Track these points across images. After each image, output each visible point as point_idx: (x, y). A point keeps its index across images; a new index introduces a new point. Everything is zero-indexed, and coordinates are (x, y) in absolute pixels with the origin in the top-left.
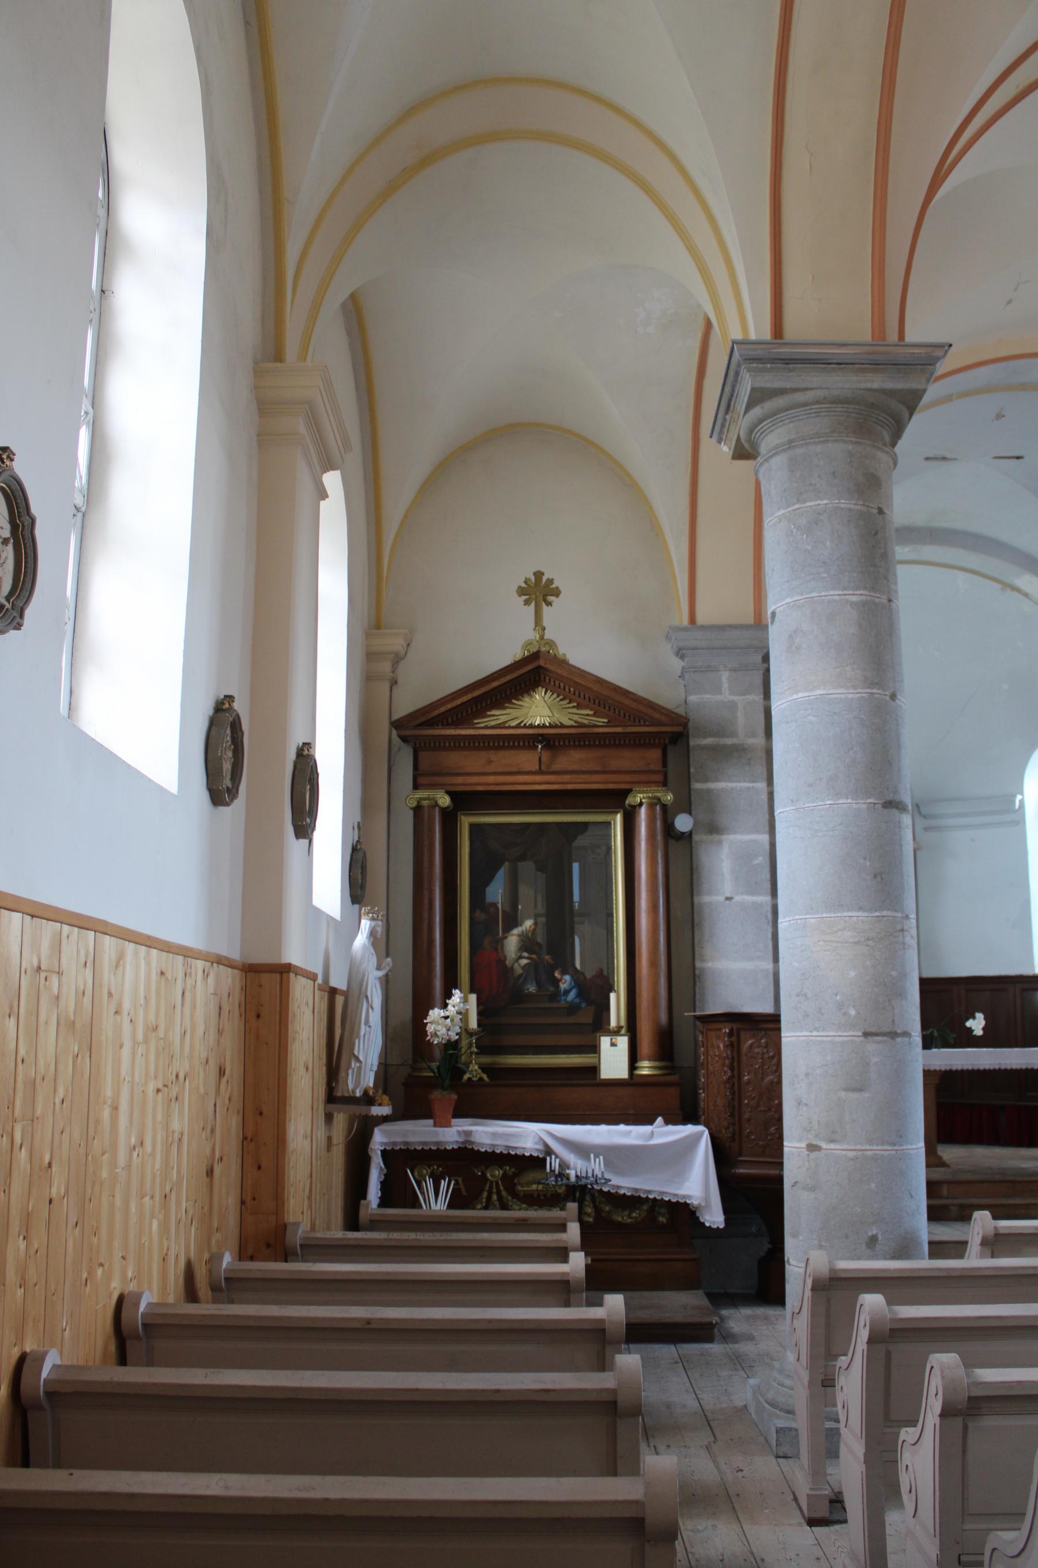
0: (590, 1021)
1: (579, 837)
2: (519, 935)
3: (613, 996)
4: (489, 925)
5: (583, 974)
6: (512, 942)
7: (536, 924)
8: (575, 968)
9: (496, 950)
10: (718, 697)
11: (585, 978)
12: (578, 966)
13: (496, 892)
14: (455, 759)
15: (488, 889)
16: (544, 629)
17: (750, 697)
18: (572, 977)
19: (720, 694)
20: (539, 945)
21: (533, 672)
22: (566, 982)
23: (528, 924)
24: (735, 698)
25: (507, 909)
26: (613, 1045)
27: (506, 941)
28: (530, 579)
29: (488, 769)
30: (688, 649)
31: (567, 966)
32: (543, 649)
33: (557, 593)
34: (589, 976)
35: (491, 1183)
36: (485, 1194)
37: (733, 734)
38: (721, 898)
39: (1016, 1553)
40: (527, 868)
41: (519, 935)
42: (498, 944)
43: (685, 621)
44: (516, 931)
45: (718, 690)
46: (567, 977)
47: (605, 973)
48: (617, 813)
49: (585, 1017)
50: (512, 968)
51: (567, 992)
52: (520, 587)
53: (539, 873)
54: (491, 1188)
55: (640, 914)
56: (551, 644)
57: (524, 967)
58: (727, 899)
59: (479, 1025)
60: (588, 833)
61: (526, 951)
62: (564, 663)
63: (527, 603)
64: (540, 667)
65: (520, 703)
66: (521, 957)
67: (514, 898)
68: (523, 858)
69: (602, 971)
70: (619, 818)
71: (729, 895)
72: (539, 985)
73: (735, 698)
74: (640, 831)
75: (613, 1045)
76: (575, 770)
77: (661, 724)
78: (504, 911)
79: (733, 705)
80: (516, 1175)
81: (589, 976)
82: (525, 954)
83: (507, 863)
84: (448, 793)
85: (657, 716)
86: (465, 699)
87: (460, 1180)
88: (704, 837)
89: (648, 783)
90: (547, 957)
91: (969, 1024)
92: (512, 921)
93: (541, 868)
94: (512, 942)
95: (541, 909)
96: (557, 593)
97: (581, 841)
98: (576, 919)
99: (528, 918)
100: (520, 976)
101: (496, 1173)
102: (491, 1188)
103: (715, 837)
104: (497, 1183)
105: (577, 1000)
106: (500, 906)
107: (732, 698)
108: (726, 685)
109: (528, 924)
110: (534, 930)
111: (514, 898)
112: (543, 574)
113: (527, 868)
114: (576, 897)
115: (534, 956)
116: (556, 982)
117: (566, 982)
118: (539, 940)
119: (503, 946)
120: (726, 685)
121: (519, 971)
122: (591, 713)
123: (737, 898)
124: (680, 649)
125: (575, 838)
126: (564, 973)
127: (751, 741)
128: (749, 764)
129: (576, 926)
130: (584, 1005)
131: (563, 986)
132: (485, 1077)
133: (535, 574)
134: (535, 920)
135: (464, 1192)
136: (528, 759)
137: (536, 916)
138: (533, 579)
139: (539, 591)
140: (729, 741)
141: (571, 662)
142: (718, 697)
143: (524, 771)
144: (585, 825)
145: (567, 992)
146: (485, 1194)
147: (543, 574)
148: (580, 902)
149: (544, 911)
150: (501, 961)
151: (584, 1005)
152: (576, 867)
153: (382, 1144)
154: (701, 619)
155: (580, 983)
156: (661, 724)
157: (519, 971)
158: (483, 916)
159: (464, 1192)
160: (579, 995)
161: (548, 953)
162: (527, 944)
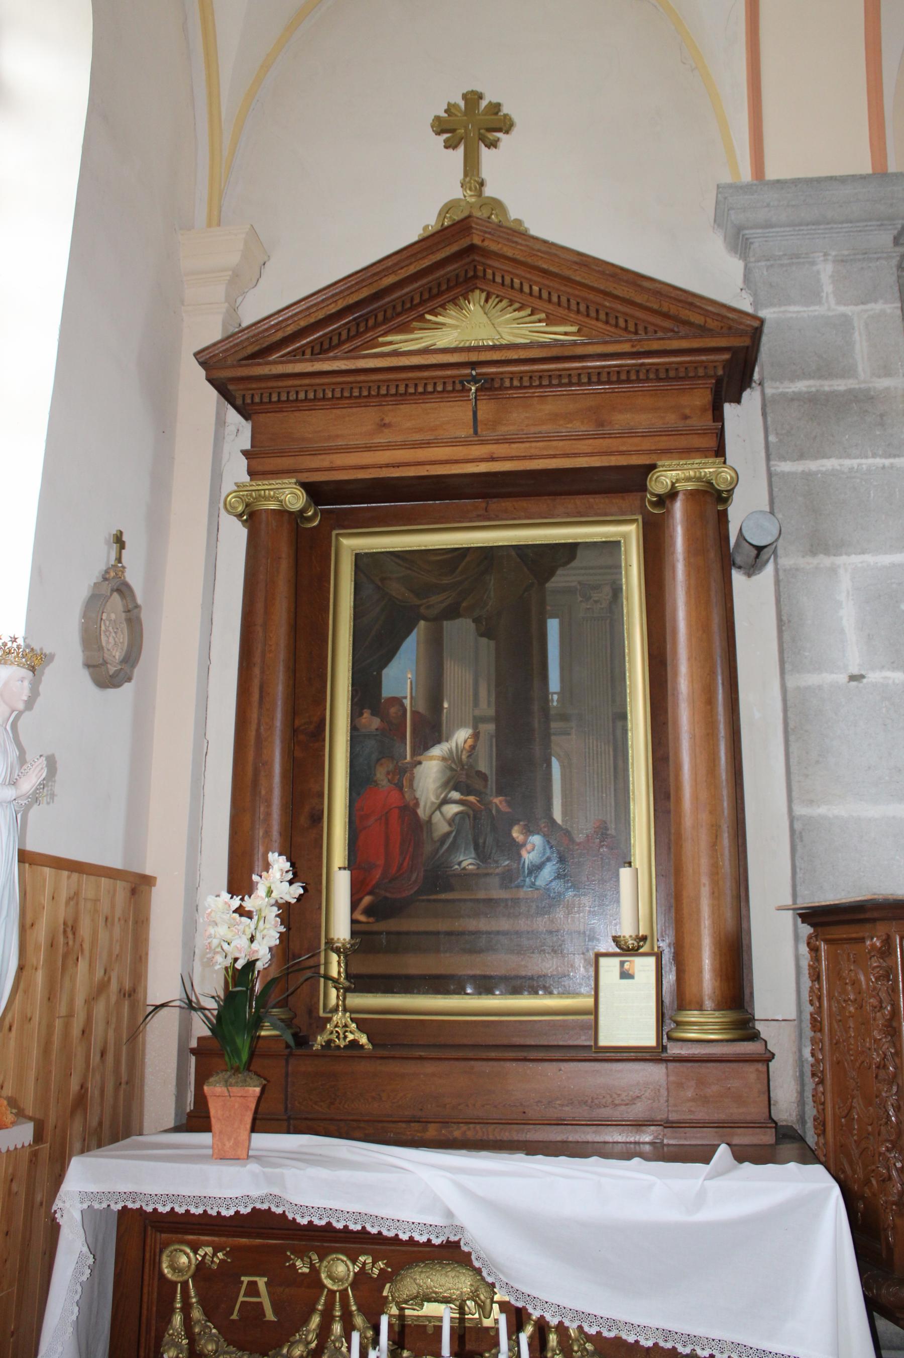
2: (444, 759)
4: (388, 735)
6: (430, 774)
7: (476, 736)
8: (553, 822)
9: (400, 787)
10: (816, 310)
13: (402, 677)
14: (314, 424)
15: (385, 672)
16: (482, 184)
17: (877, 307)
19: (820, 303)
20: (483, 777)
21: (464, 256)
23: (462, 736)
24: (847, 310)
25: (422, 708)
26: (625, 975)
27: (418, 770)
28: (456, 106)
29: (381, 439)
30: (756, 226)
32: (477, 213)
33: (506, 125)
35: (332, 1293)
36: (315, 1321)
37: (849, 372)
38: (842, 678)
41: (444, 759)
42: (403, 775)
43: (746, 175)
44: (437, 751)
45: (813, 295)
46: (536, 840)
50: (429, 821)
51: (537, 868)
52: (437, 118)
53: (484, 640)
54: (329, 1306)
55: (676, 705)
56: (496, 205)
57: (451, 822)
58: (853, 678)
59: (353, 933)
60: (574, 564)
61: (456, 788)
62: (517, 233)
63: (450, 145)
64: (472, 248)
65: (440, 319)
66: (445, 801)
67: (435, 692)
68: (452, 612)
70: (629, 534)
71: (855, 671)
73: (847, 310)
74: (673, 544)
75: (625, 975)
76: (541, 435)
77: (703, 331)
78: (414, 713)
79: (844, 324)
80: (385, 1278)
82: (455, 795)
83: (422, 623)
84: (305, 486)
85: (698, 319)
86: (494, 750)
87: (261, 1282)
88: (809, 562)
89: (687, 452)
92: (431, 731)
93: (486, 631)
94: (430, 774)
95: (487, 708)
96: (506, 125)
97: (561, 579)
98: (553, 725)
99: (462, 725)
100: (448, 834)
101: (340, 1270)
102: (329, 1306)
103: (825, 561)
104: (344, 1293)
106: (407, 703)
107: (842, 309)
108: (828, 288)
109: (462, 736)
110: (473, 747)
111: (435, 692)
112: (480, 97)
113: (461, 631)
114: (554, 683)
115: (471, 798)
116: (514, 849)
118: (483, 766)
119: (411, 780)
120: (828, 288)
121: (442, 827)
122: (574, 329)
123: (873, 677)
124: (739, 229)
125: (551, 573)
127: (883, 383)
128: (882, 425)
131: (529, 857)
132: (363, 1040)
133: (465, 96)
134: (475, 727)
135: (270, 1315)
136: (453, 416)
137: (476, 722)
138: (462, 104)
139: (473, 126)
140: (840, 385)
141: (533, 232)
142: (816, 310)
143: (443, 440)
144: (570, 550)
145: (537, 868)
146: (315, 1321)
147: (480, 97)
148: (561, 693)
149: (491, 712)
150: (409, 810)
152: (553, 626)
153: (84, 1196)
154: (772, 173)
156: (703, 331)
157: (442, 827)
158: (376, 723)
159: (270, 1315)
161: (500, 792)
162: (461, 777)
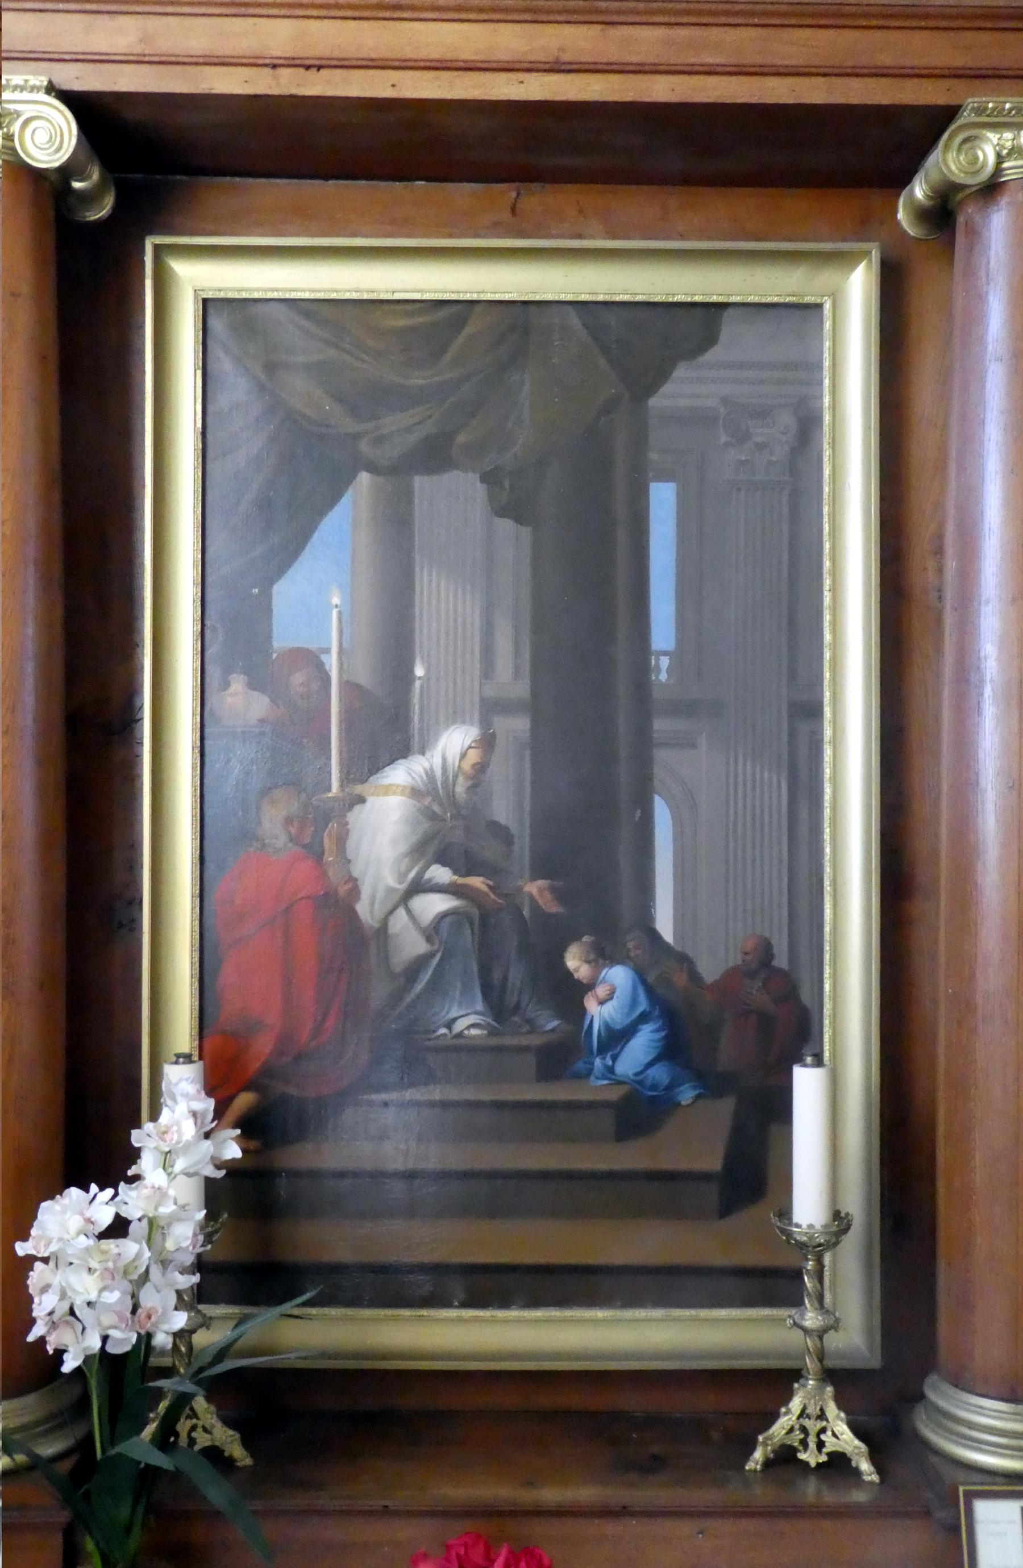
0: (713, 1162)
1: (681, 371)
2: (415, 793)
3: (807, 1084)
5: (685, 960)
7: (487, 742)
8: (655, 936)
11: (694, 976)
12: (665, 925)
18: (640, 975)
20: (502, 834)
22: (612, 994)
23: (454, 743)
25: (364, 678)
27: (357, 817)
31: (610, 915)
34: (710, 970)
39: (37, 132)
40: (453, 501)
41: (415, 793)
44: (400, 774)
47: (781, 961)
48: (846, 260)
49: (695, 1139)
50: (383, 931)
51: (616, 1038)
53: (506, 526)
57: (432, 932)
61: (442, 859)
66: (419, 887)
68: (435, 455)
69: (766, 949)
72: (499, 1007)
78: (349, 687)
81: (710, 970)
82: (441, 874)
83: (364, 478)
90: (534, 888)
91: (239, 1154)
92: (385, 731)
93: (513, 504)
95: (512, 679)
97: (685, 388)
98: (660, 725)
99: (456, 717)
100: (419, 964)
105: (660, 1074)
106: (332, 663)
109: (454, 743)
110: (481, 768)
115: (477, 882)
116: (569, 995)
117: (612, 994)
119: (342, 840)
125: (662, 375)
126: (604, 955)
129: (660, 755)
130: (686, 1095)
131: (601, 1012)
134: (485, 723)
137: (490, 710)
144: (709, 315)
145: (616, 1038)
148: (677, 656)
149: (522, 690)
151: (686, 1095)
152: (663, 500)
155: (681, 1016)
160: (672, 1050)
161: (541, 868)
162: (450, 834)
